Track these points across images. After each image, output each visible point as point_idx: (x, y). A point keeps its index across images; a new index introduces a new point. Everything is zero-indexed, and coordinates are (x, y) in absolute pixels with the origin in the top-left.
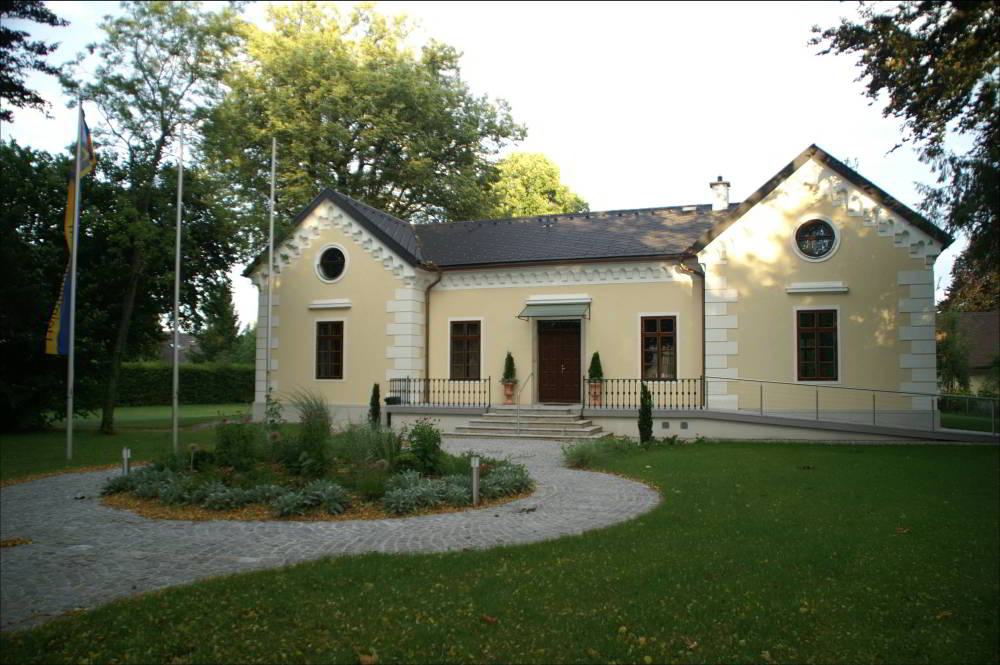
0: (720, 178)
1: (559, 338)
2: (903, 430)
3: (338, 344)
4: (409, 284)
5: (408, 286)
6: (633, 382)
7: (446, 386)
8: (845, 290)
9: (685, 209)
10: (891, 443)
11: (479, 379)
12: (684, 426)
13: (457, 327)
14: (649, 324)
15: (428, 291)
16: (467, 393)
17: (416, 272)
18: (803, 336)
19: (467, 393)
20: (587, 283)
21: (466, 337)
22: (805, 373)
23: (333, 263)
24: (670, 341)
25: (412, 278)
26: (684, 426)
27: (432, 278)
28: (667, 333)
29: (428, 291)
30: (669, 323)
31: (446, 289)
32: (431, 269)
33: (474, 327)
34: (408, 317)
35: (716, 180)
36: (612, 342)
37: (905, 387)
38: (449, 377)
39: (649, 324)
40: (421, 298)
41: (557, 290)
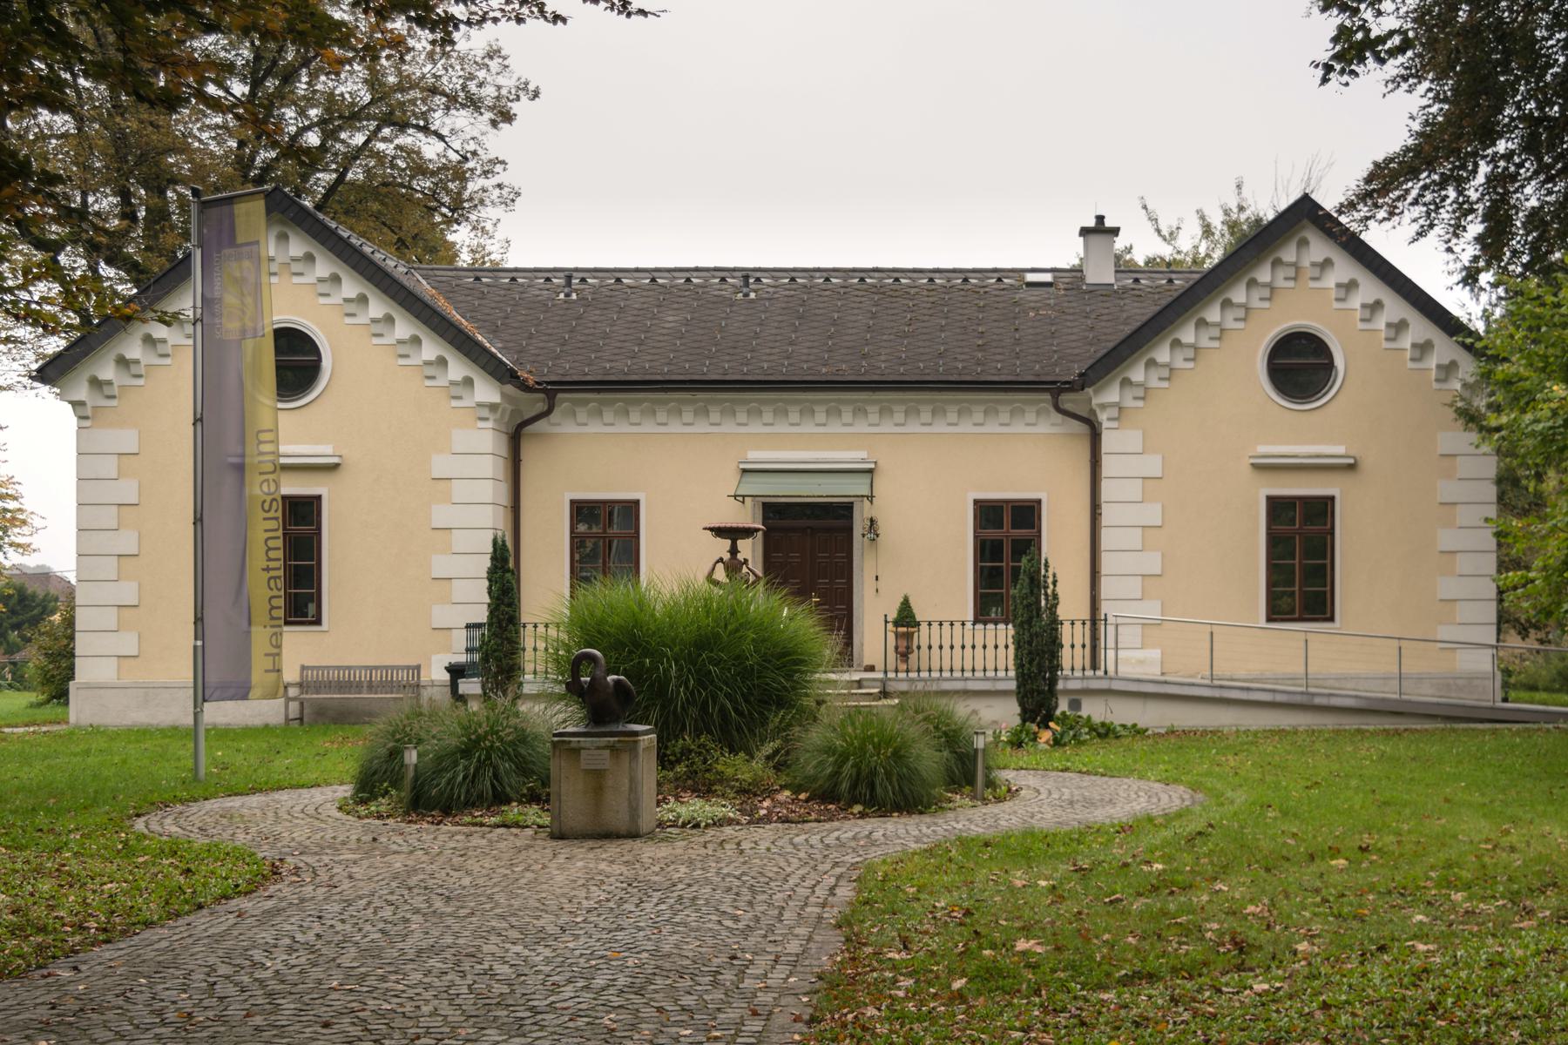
0: (1100, 219)
2: (1438, 704)
4: (486, 419)
5: (481, 424)
6: (958, 626)
7: (968, 635)
8: (1351, 461)
9: (1030, 277)
13: (583, 511)
14: (988, 513)
15: (516, 438)
16: (979, 649)
17: (503, 395)
18: (1277, 544)
19: (979, 649)
22: (1276, 612)
24: (1028, 546)
25: (493, 407)
28: (991, 533)
30: (1027, 513)
31: (556, 430)
35: (1092, 223)
37: (1444, 633)
38: (971, 617)
39: (988, 513)
41: (807, 448)
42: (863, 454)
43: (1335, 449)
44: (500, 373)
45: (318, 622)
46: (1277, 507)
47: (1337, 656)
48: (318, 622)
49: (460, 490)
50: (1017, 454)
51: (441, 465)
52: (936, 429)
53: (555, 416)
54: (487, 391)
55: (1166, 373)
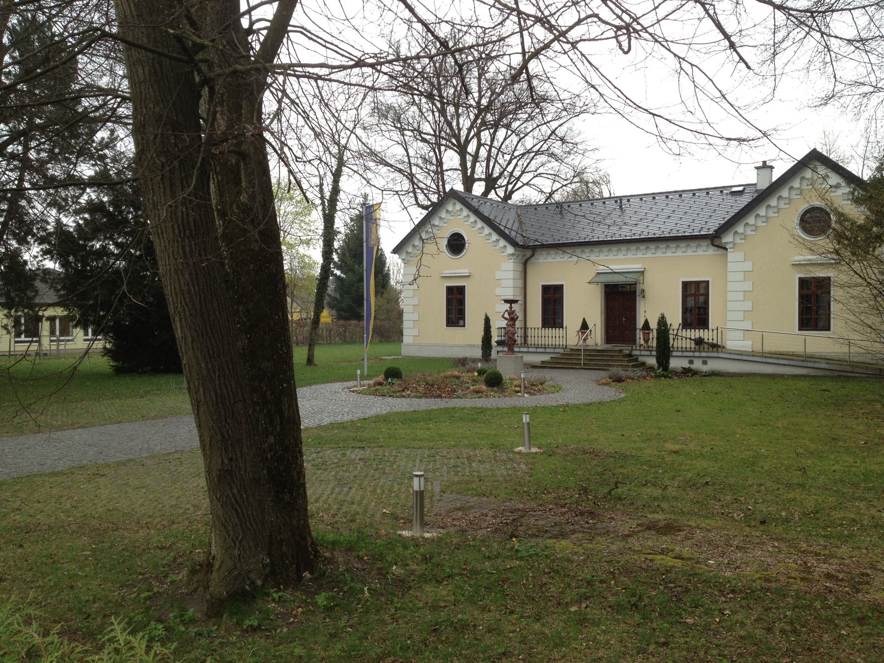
0: (764, 162)
1: (620, 298)
3: (462, 302)
9: (734, 189)
10: (813, 374)
11: (708, 328)
12: (705, 363)
13: (546, 289)
15: (525, 264)
18: (449, 302)
20: (702, 253)
21: (553, 297)
23: (456, 244)
26: (705, 363)
27: (529, 253)
28: (805, 291)
29: (525, 264)
32: (525, 247)
33: (559, 289)
34: (511, 283)
36: (660, 304)
40: (520, 268)
42: (640, 266)
43: (465, 271)
44: (514, 243)
45: (464, 326)
46: (450, 290)
47: (817, 343)
48: (464, 326)
49: (504, 283)
50: (695, 264)
51: (498, 275)
52: (628, 257)
53: (536, 256)
54: (510, 250)
55: (754, 228)
